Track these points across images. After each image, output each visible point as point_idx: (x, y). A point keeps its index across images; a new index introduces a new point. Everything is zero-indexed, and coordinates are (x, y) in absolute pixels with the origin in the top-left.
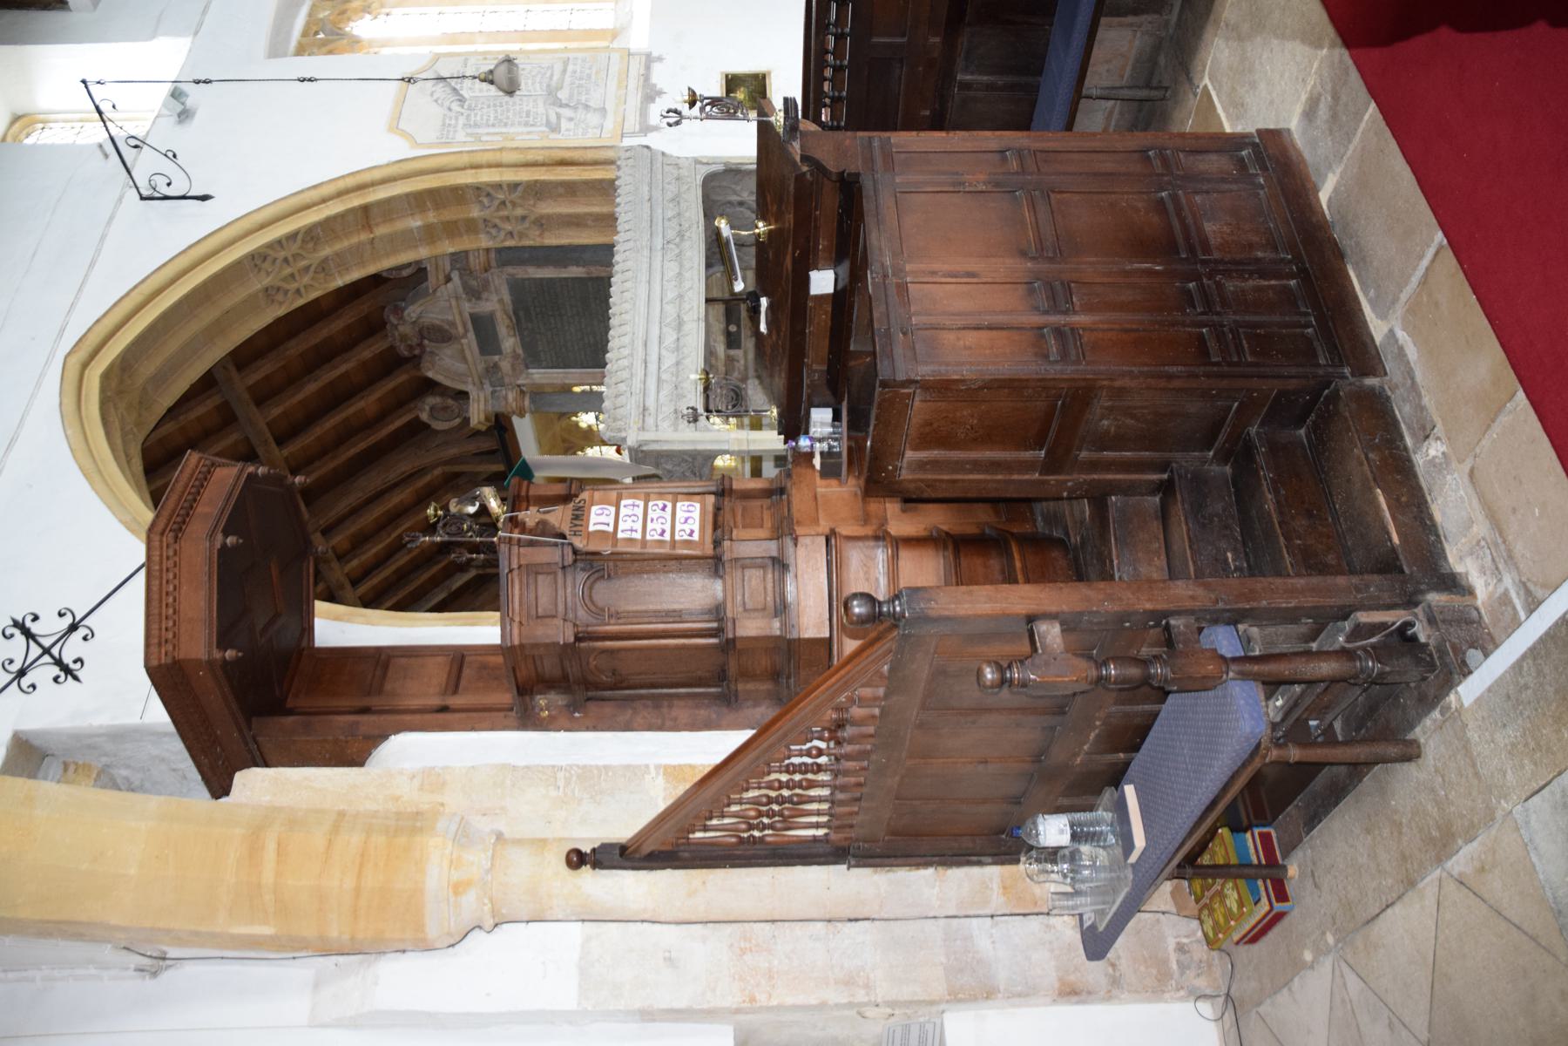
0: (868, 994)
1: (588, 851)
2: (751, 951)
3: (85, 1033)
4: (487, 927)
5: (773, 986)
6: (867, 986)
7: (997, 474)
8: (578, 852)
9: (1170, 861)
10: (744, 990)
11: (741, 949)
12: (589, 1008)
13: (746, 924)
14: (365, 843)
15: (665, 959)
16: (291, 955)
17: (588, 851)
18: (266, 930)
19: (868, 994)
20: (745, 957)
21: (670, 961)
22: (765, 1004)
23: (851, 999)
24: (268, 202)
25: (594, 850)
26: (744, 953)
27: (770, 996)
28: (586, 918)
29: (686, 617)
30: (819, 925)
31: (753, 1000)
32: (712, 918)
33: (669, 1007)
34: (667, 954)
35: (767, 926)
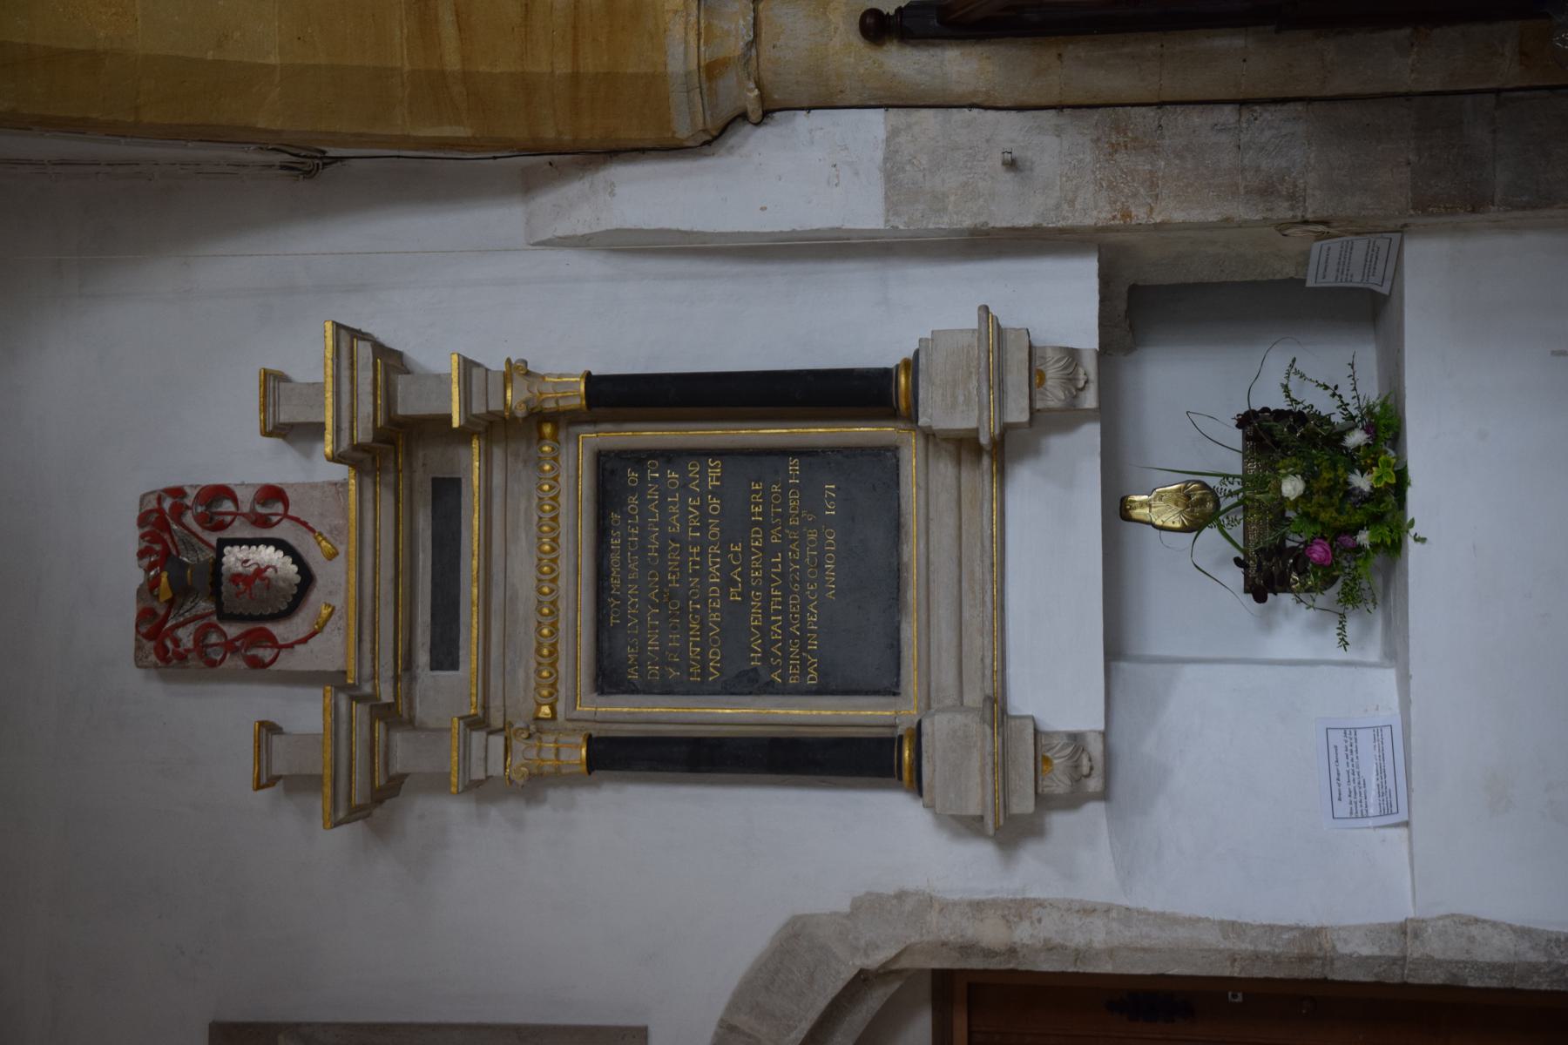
0: (1292, 208)
1: (892, 12)
2: (1126, 146)
3: (243, 255)
4: (755, 117)
5: (1157, 196)
6: (1292, 197)
7: (871, 715)
8: (874, 13)
9: (1326, 262)
10: (1115, 202)
11: (1113, 145)
12: (901, 227)
13: (1120, 110)
14: (576, 8)
15: (1004, 163)
16: (492, 155)
17: (892, 12)
18: (461, 132)
19: (1292, 208)
20: (1117, 156)
21: (1012, 165)
22: (1144, 222)
23: (1268, 214)
24: (858, 110)
25: (899, 10)
26: (1116, 151)
27: (1152, 209)
28: (890, 103)
29: (1001, 730)
30: (1228, 109)
31: (1127, 215)
32: (1070, 101)
33: (1009, 225)
34: (1008, 157)
35: (1151, 113)
